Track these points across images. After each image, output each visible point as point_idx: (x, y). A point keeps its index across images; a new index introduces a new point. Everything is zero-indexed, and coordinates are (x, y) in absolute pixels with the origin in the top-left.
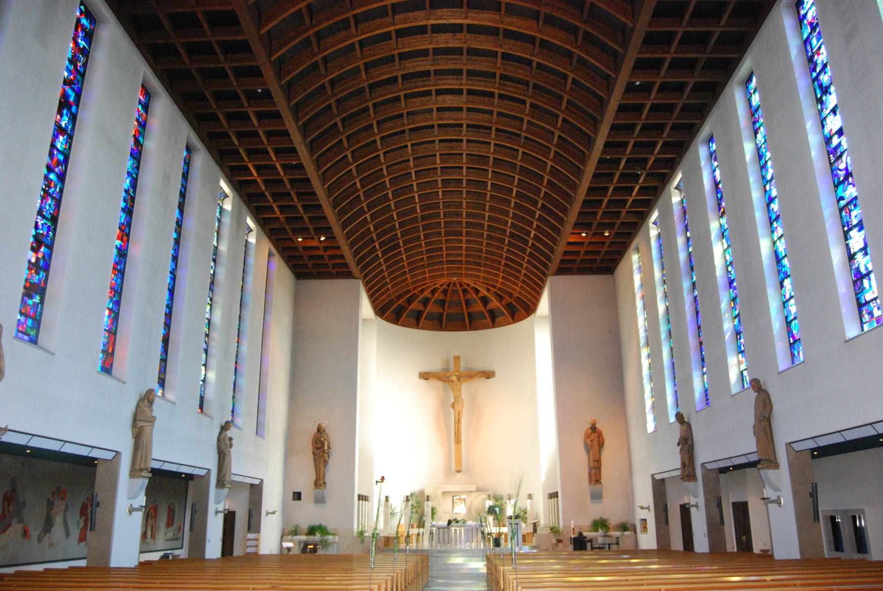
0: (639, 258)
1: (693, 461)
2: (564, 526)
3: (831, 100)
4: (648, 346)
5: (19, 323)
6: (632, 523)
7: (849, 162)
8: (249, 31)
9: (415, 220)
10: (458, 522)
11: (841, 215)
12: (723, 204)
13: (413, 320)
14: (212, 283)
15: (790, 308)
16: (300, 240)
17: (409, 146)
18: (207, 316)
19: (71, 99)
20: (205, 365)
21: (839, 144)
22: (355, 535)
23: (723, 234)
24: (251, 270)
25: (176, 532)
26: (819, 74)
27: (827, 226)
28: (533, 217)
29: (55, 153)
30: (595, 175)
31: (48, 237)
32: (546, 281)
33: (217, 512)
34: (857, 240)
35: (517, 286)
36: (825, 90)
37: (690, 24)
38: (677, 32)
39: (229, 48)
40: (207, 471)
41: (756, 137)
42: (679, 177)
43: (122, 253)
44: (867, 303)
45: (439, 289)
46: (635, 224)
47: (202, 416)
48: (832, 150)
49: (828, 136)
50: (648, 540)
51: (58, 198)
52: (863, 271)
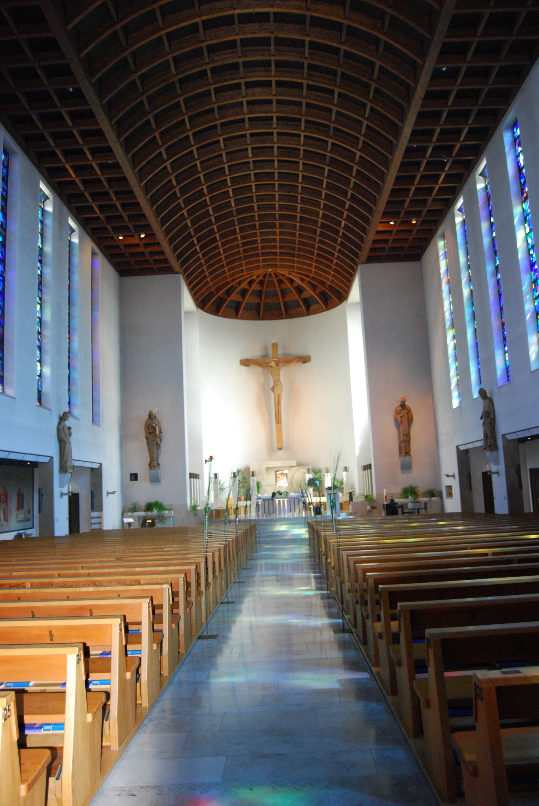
0: (445, 244)
4: (453, 328)
6: (438, 490)
9: (230, 214)
14: (40, 283)
16: (121, 238)
17: (222, 141)
18: (38, 315)
20: (40, 361)
22: (189, 509)
23: (525, 218)
25: (26, 514)
32: (357, 269)
33: (62, 495)
40: (49, 458)
47: (40, 409)
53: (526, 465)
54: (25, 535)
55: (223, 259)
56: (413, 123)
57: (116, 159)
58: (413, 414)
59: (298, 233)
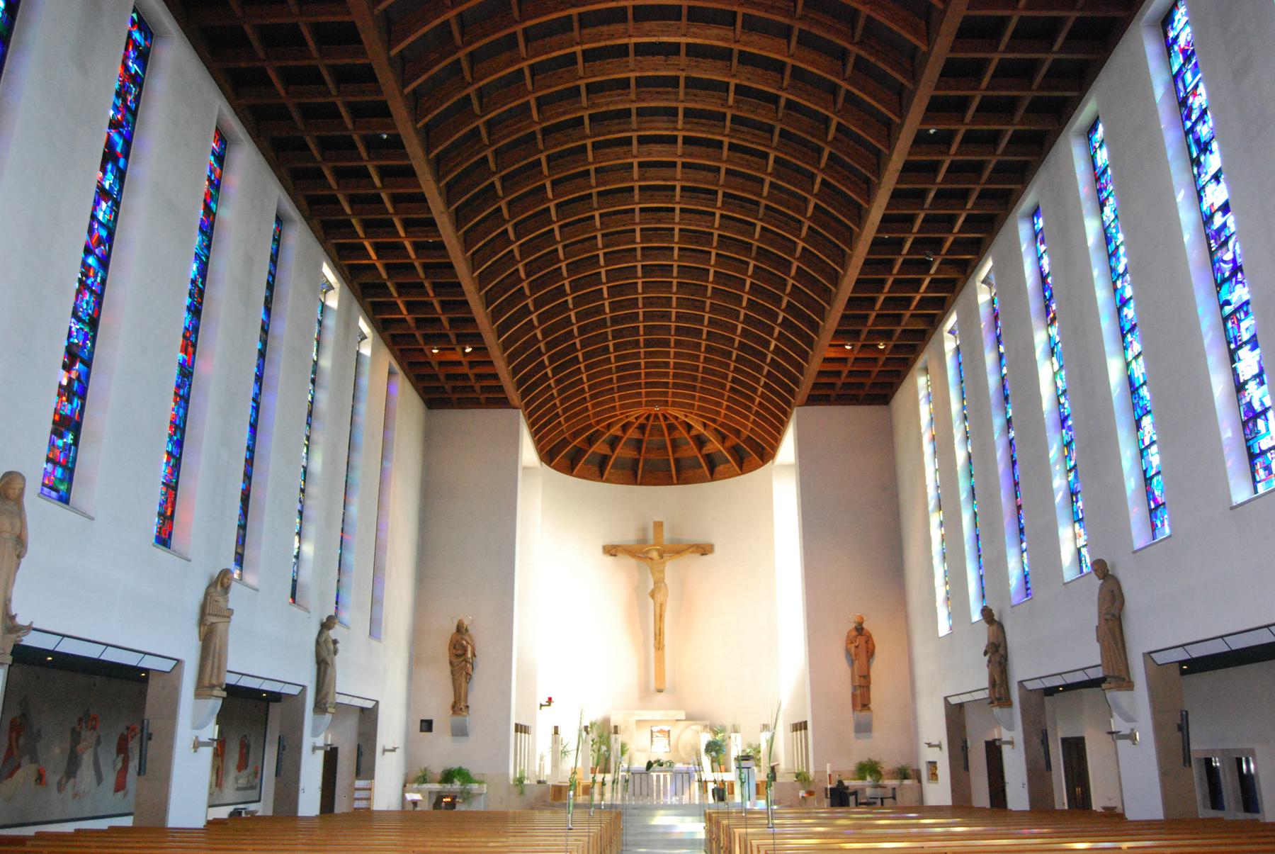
0: (928, 381)
1: (1006, 676)
2: (816, 772)
3: (1213, 162)
4: (940, 509)
5: (46, 474)
6: (915, 768)
7: (1238, 251)
8: (375, 52)
9: (603, 323)
10: (661, 765)
11: (1225, 326)
12: (1054, 307)
13: (595, 469)
14: (310, 414)
15: (1151, 459)
16: (435, 351)
17: (597, 218)
18: (304, 463)
19: (119, 149)
20: (299, 534)
21: (1224, 225)
22: (512, 782)
23: (1052, 350)
24: (364, 396)
25: (250, 778)
26: (1195, 124)
27: (1206, 342)
28: (775, 321)
29: (96, 227)
30: (867, 262)
31: (85, 348)
32: (791, 413)
33: (315, 749)
34: (1248, 362)
35: (748, 420)
36: (1204, 148)
37: (1009, 49)
38: (990, 60)
39: (345, 76)
40: (301, 688)
41: (1102, 211)
42: (988, 265)
43: (186, 371)
44: (1263, 453)
45: (633, 423)
46: (923, 332)
47: (294, 609)
48: (1213, 233)
49: (1208, 213)
50: (939, 792)
51: (99, 292)
52: (1258, 408)
53: (1056, 733)
54: (246, 813)
55: (587, 389)
56: (884, 205)
57: (440, 236)
58: (876, 644)
59: (702, 356)
